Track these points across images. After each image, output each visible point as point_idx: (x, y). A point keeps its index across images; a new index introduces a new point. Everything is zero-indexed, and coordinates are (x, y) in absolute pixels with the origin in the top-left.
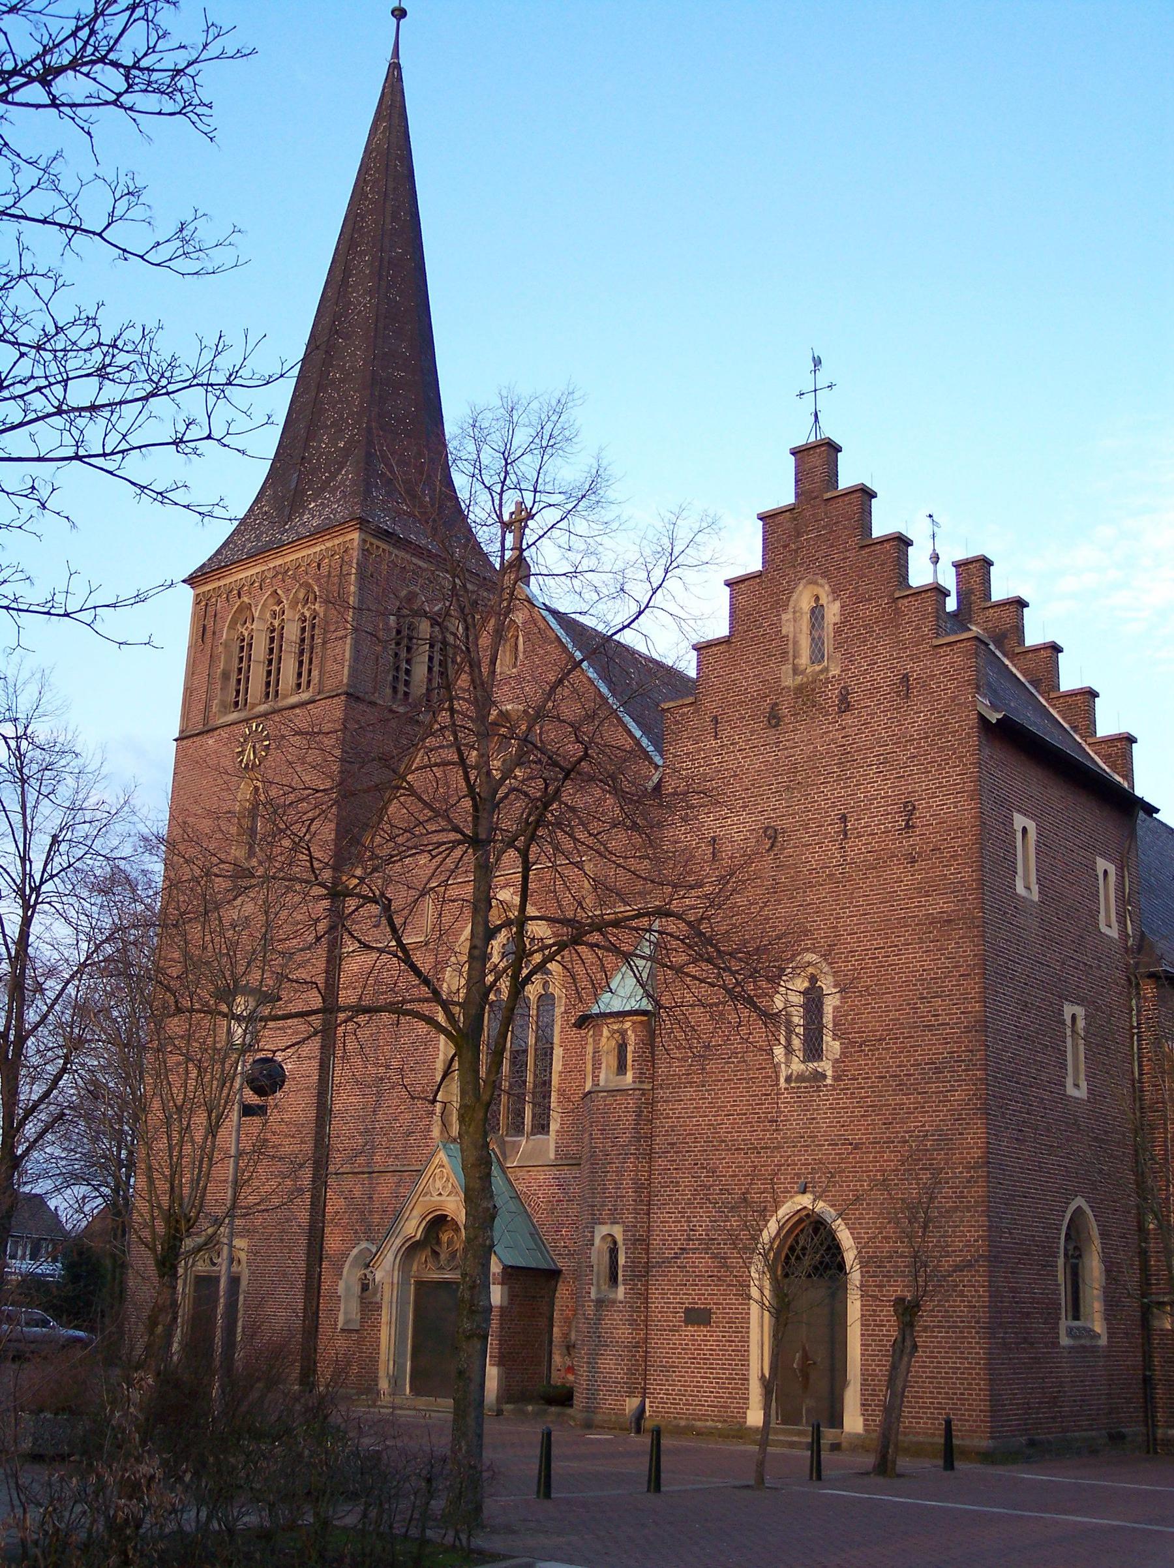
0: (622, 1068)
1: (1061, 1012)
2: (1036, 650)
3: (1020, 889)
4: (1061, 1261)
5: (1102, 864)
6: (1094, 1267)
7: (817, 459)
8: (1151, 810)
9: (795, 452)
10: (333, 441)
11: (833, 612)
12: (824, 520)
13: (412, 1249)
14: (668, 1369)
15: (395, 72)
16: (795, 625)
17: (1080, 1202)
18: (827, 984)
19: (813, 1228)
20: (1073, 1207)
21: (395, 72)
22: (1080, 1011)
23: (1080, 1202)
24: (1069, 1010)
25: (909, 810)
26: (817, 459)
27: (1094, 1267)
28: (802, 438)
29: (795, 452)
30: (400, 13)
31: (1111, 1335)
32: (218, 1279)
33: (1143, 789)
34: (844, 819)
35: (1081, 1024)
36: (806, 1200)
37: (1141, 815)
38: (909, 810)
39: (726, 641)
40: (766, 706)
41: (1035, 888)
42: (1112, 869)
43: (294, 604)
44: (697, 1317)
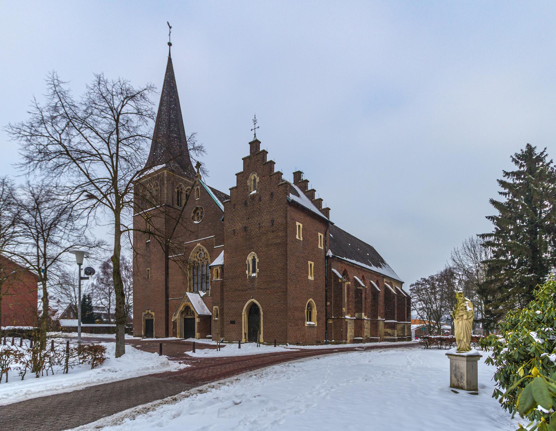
0: (218, 277)
1: (307, 263)
2: (310, 191)
3: (297, 237)
4: (306, 311)
5: (319, 234)
6: (315, 312)
7: (255, 144)
8: (332, 224)
9: (250, 143)
10: (160, 150)
11: (258, 180)
12: (257, 159)
13: (182, 313)
14: (483, 387)
15: (170, 60)
16: (250, 183)
17: (311, 299)
18: (256, 257)
19: (253, 305)
20: (309, 300)
21: (170, 60)
22: (313, 263)
23: (311, 299)
24: (309, 262)
25: (272, 221)
26: (255, 144)
27: (315, 312)
28: (252, 140)
29: (250, 143)
30: (170, 44)
31: (318, 324)
32: (153, 320)
33: (331, 219)
34: (260, 224)
35: (313, 266)
36: (253, 300)
37: (330, 225)
38: (272, 221)
39: (236, 187)
40: (244, 201)
41: (301, 238)
42: (322, 235)
43: (154, 187)
44: (233, 322)
